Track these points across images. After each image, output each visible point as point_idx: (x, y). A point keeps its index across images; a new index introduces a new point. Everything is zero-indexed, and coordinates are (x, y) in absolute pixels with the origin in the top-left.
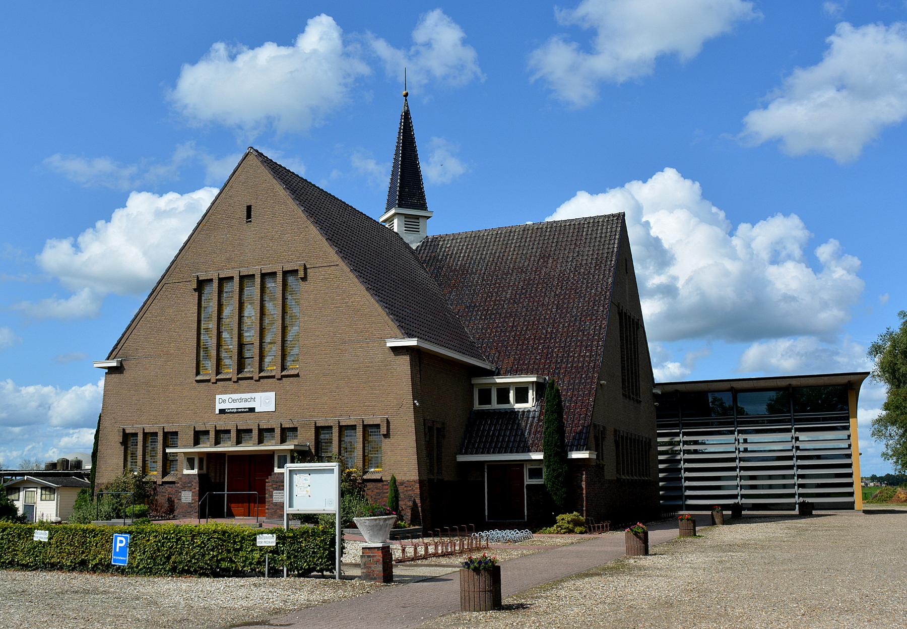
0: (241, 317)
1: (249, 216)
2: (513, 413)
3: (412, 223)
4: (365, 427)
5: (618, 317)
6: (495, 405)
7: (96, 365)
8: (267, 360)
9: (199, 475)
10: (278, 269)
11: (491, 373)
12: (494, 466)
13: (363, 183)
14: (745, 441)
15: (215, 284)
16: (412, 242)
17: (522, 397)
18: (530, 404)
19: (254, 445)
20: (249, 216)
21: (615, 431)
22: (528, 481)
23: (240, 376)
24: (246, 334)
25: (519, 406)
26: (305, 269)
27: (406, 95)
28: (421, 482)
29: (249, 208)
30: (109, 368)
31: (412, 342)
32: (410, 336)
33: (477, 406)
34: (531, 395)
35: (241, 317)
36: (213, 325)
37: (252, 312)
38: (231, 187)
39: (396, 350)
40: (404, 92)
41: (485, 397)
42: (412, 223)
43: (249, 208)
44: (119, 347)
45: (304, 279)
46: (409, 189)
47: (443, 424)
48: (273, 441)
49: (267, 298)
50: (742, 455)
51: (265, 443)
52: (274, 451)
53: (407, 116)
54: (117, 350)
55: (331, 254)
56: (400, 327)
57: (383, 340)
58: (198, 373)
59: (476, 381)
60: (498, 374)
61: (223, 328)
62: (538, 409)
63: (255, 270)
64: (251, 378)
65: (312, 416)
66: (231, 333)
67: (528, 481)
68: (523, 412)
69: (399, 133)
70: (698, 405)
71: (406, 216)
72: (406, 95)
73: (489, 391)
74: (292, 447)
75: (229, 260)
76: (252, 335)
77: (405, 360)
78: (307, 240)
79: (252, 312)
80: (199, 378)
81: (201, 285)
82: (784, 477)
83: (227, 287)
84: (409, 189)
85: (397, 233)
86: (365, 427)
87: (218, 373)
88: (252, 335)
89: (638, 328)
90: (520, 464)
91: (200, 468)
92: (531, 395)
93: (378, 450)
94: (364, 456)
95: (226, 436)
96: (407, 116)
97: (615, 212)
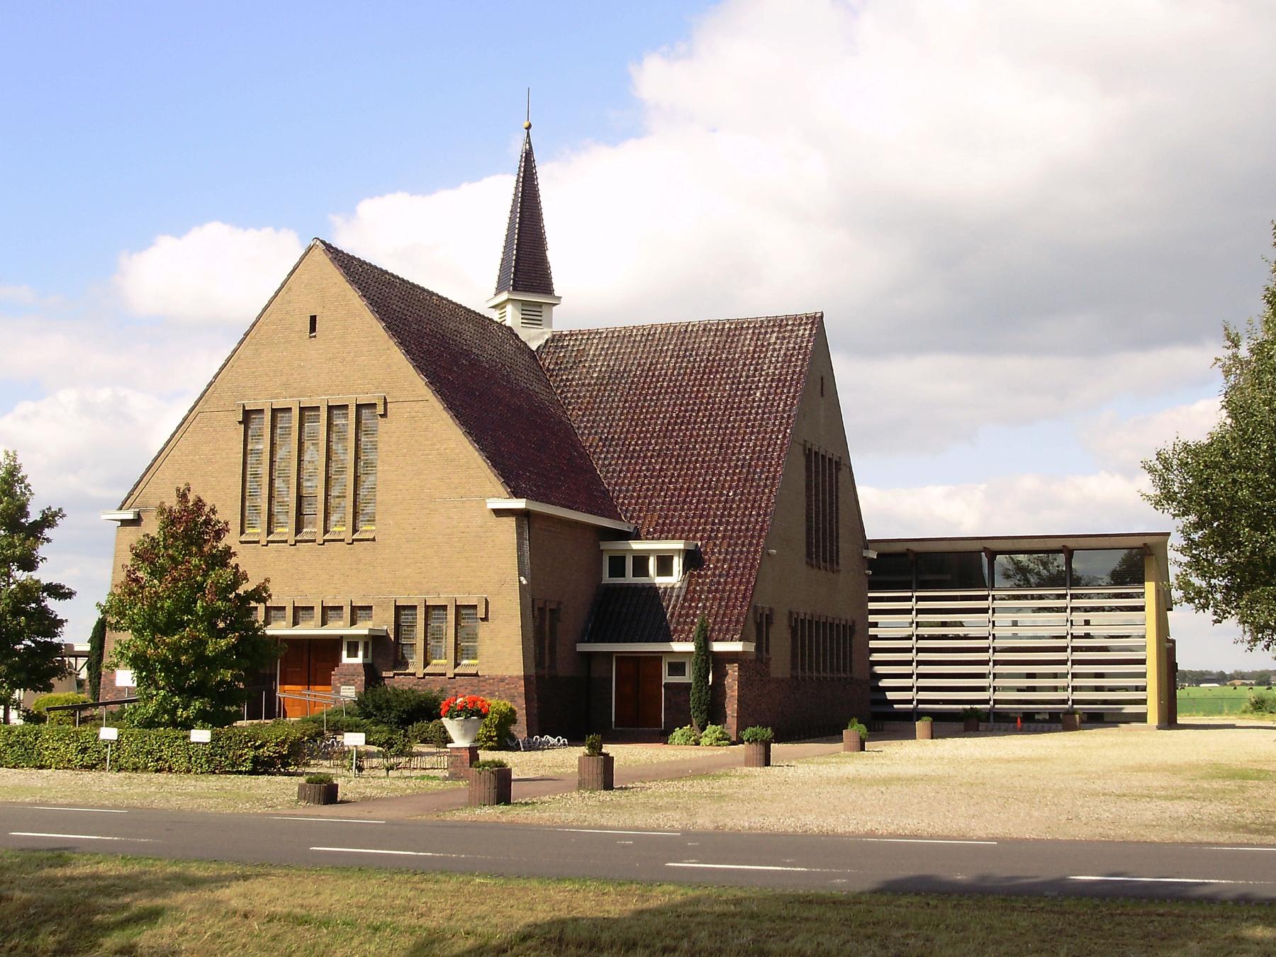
0: (300, 461)
1: (313, 329)
2: (653, 588)
3: (533, 314)
4: (458, 608)
5: (803, 461)
6: (630, 578)
7: (105, 517)
8: (334, 518)
9: (365, 665)
10: (351, 400)
11: (626, 536)
12: (623, 658)
13: (464, 271)
14: (1087, 623)
15: (268, 416)
16: (534, 339)
17: (665, 565)
18: (675, 578)
19: (316, 627)
20: (313, 329)
21: (791, 613)
22: (667, 678)
23: (298, 538)
24: (305, 484)
25: (661, 581)
26: (385, 403)
27: (528, 128)
28: (526, 678)
29: (313, 319)
30: (122, 521)
31: (520, 504)
32: (516, 494)
33: (607, 579)
34: (677, 564)
35: (300, 461)
36: (264, 470)
37: (315, 456)
38: (290, 289)
39: (499, 513)
40: (526, 124)
41: (617, 566)
42: (533, 314)
43: (313, 319)
44: (136, 493)
45: (384, 415)
46: (527, 267)
47: (559, 603)
48: (341, 623)
49: (334, 437)
50: (1077, 643)
51: (330, 624)
52: (342, 637)
53: (528, 157)
54: (133, 497)
55: (417, 384)
56: (507, 482)
57: (483, 498)
58: (242, 532)
59: (605, 545)
60: (637, 536)
61: (276, 474)
62: (685, 585)
63: (321, 401)
64: (314, 541)
65: (391, 593)
66: (287, 482)
67: (667, 678)
68: (666, 589)
69: (516, 188)
70: (947, 568)
71: (524, 303)
72: (528, 128)
73: (624, 558)
74: (366, 632)
75: (286, 385)
76: (315, 486)
77: (511, 522)
78: (389, 366)
79: (315, 456)
80: (244, 538)
81: (248, 416)
82: (1055, 676)
83: (282, 421)
84: (527, 267)
85: (510, 328)
86: (458, 608)
87: (270, 532)
88: (315, 486)
89: (838, 469)
90: (656, 658)
91: (365, 656)
92: (677, 564)
93: (473, 637)
94: (456, 644)
95: (280, 613)
96: (528, 157)
97: (810, 311)
